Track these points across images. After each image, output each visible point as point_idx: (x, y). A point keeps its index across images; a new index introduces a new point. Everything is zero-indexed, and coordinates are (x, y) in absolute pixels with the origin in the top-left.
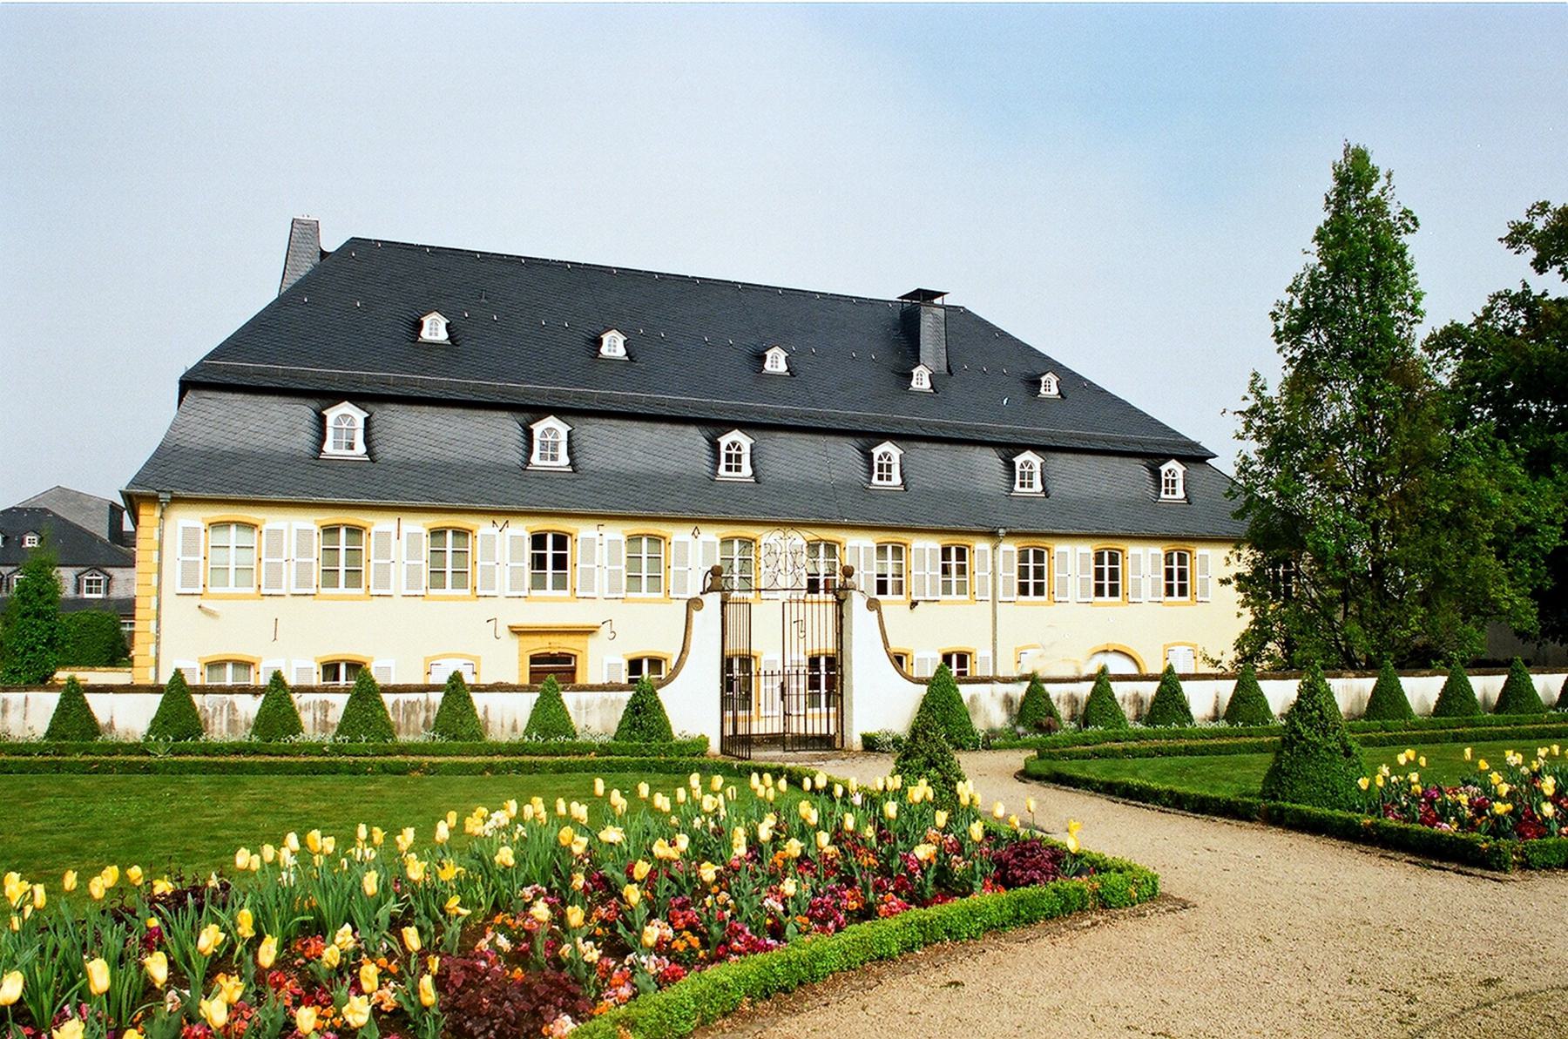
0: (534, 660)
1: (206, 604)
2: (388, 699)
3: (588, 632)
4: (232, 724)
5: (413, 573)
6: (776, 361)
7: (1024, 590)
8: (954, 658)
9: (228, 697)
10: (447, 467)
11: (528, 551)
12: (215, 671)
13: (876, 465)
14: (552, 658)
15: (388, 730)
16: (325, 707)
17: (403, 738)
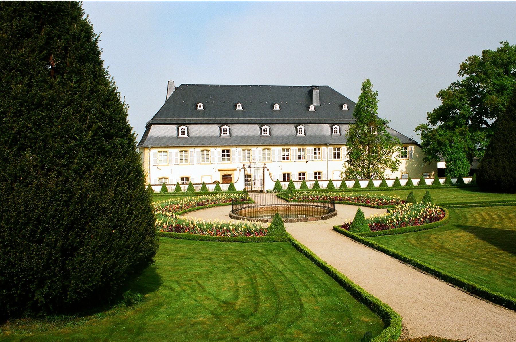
0: (223, 176)
1: (159, 167)
2: (194, 186)
3: (235, 170)
4: (171, 190)
5: (198, 159)
6: (277, 107)
7: (335, 157)
8: (317, 173)
9: (171, 186)
10: (204, 137)
11: (221, 154)
12: (161, 180)
13: (298, 131)
14: (227, 175)
15: (194, 190)
16: (185, 187)
17: (196, 191)
